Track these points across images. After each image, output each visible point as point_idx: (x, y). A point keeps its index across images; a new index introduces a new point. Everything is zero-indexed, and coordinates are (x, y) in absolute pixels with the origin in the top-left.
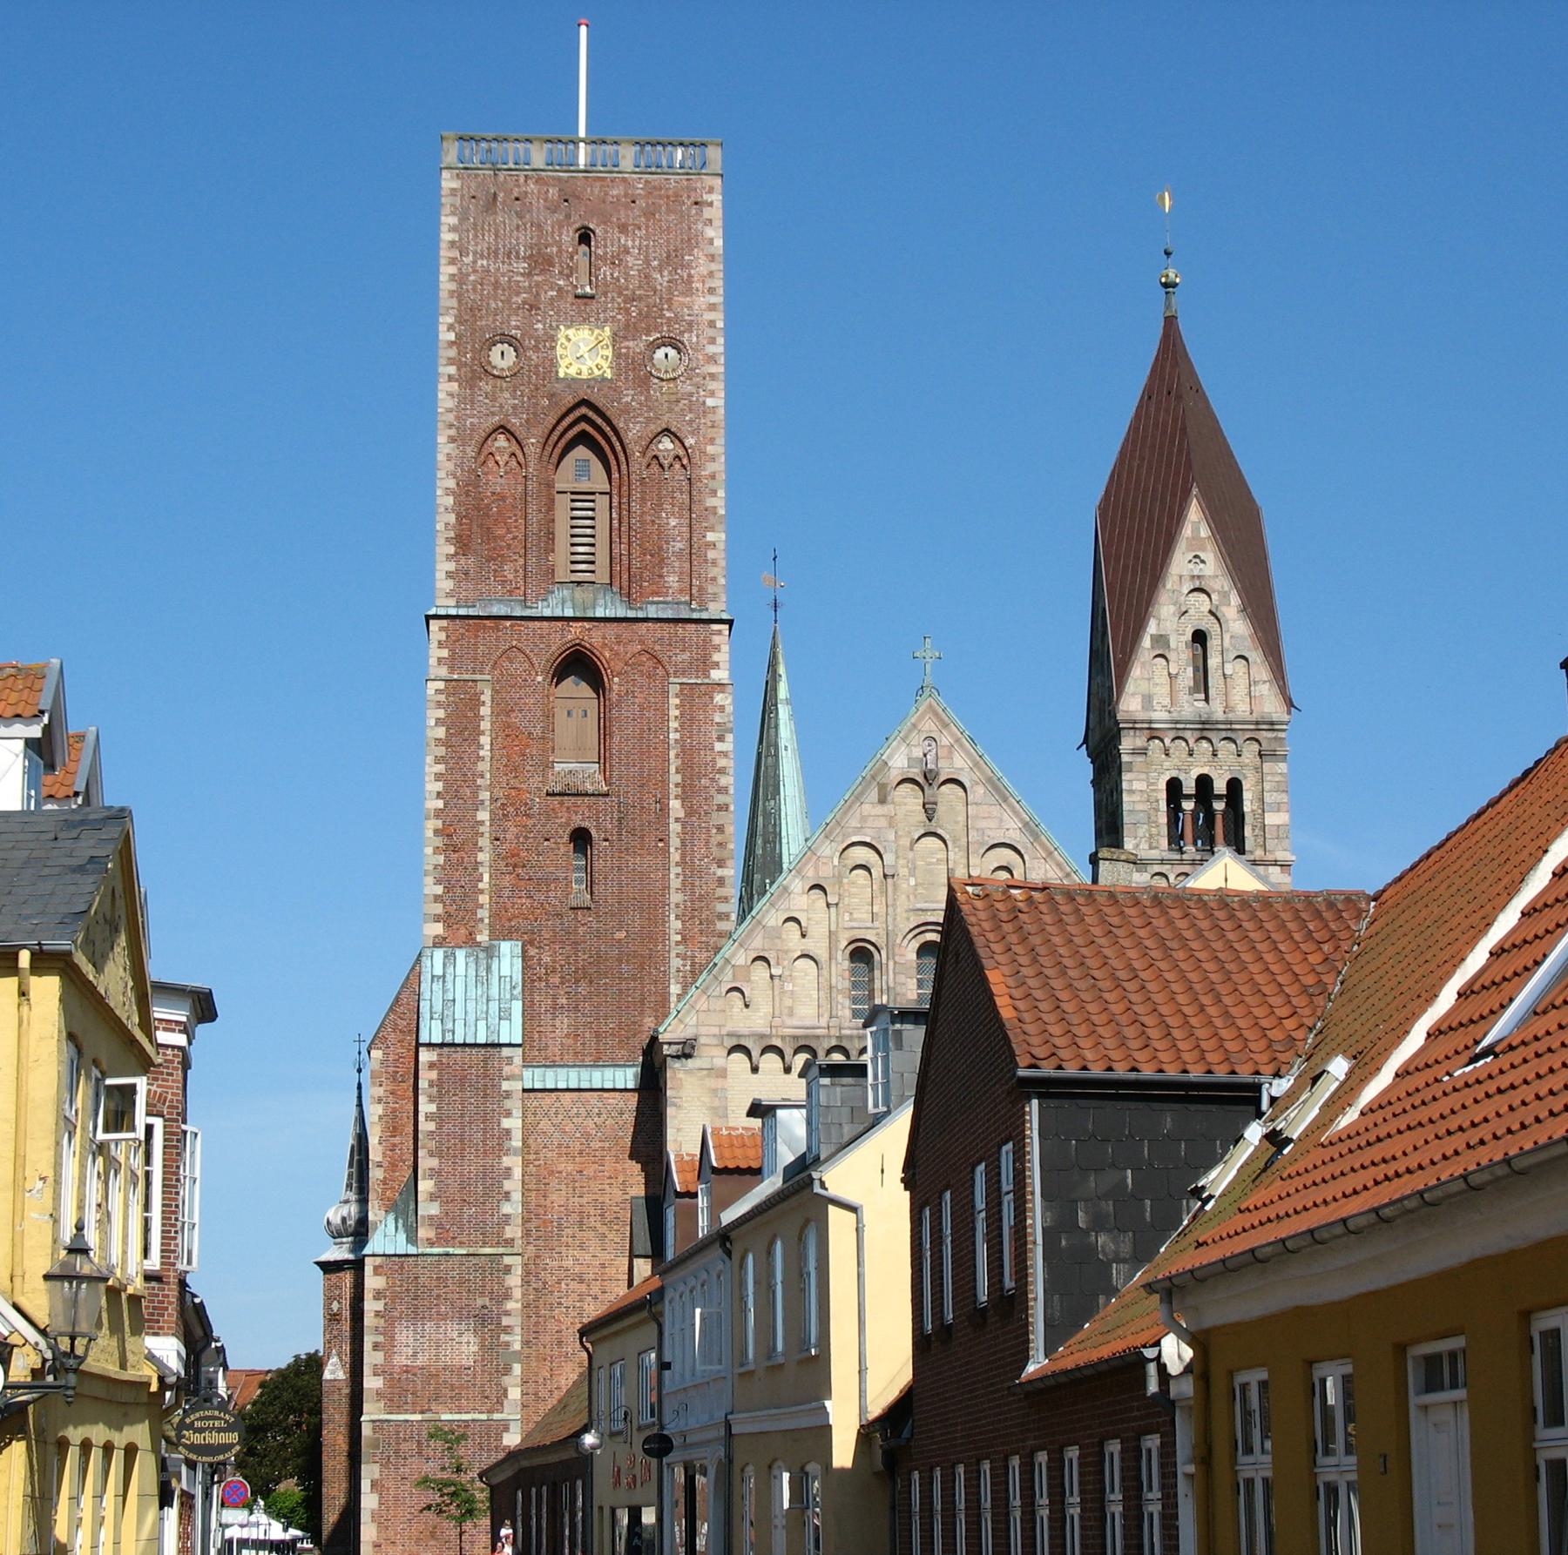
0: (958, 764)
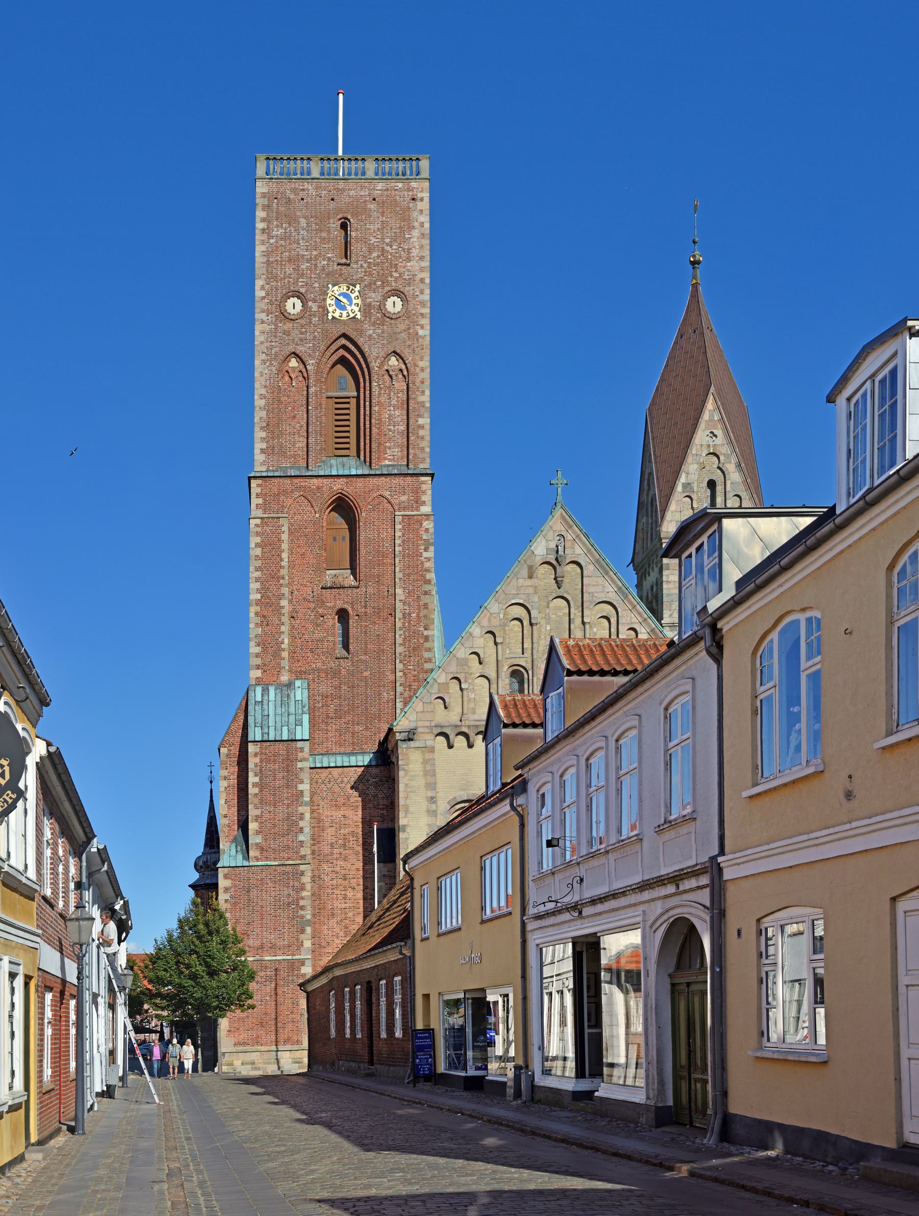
0: (577, 551)
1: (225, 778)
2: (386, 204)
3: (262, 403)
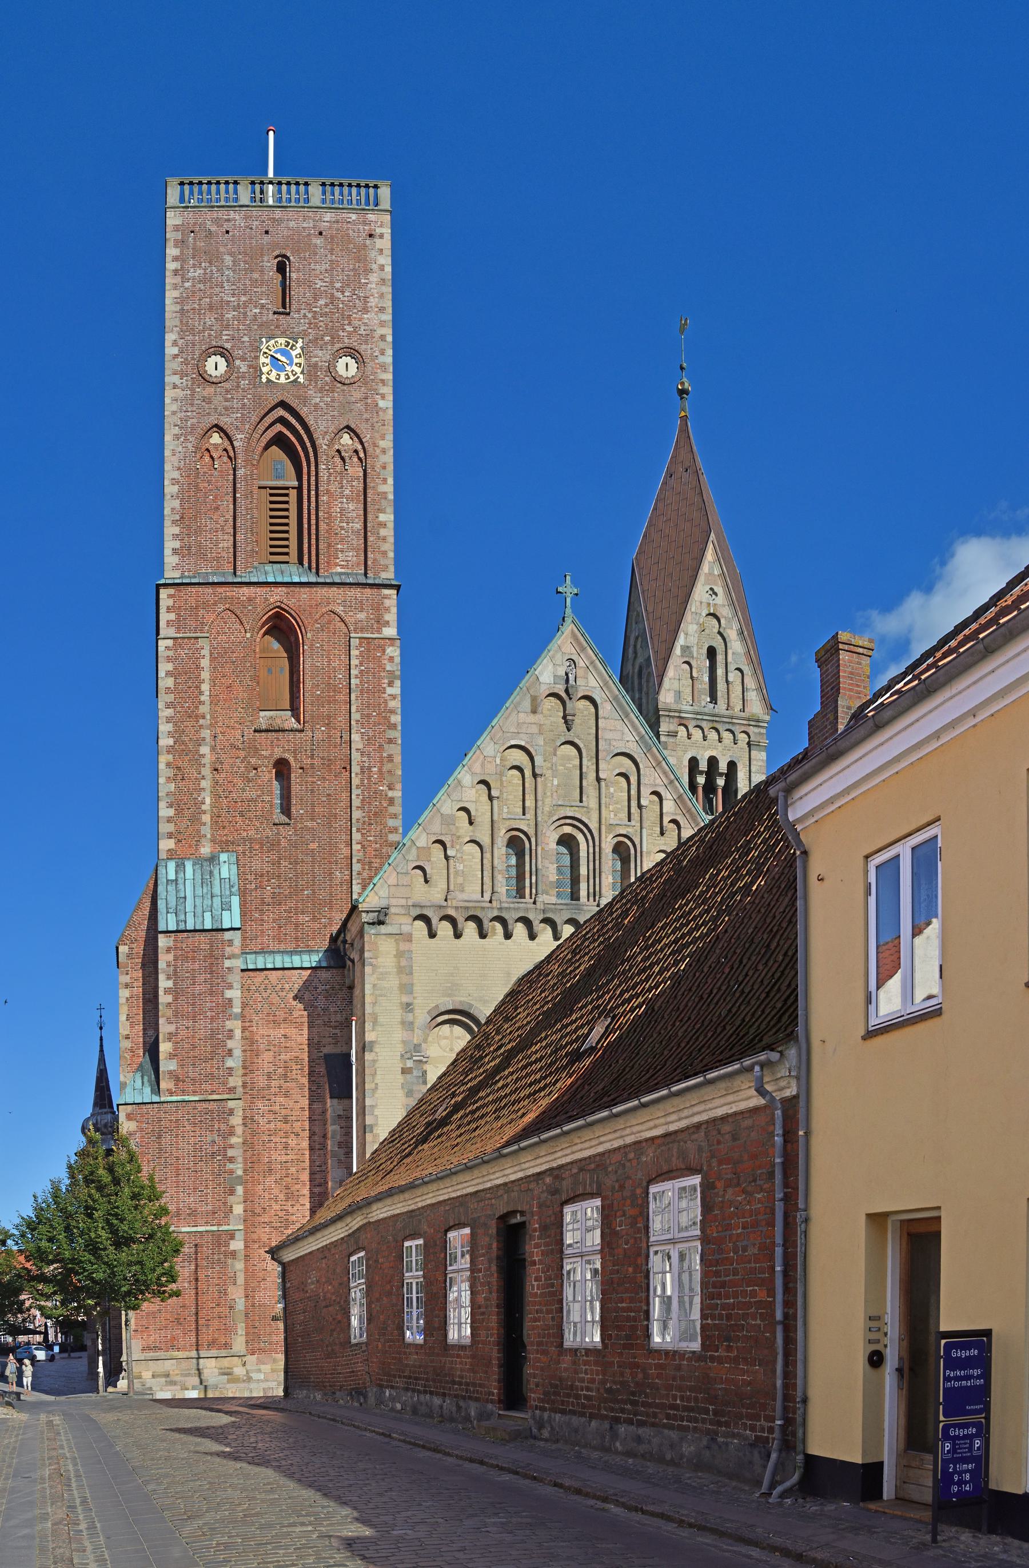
1: (127, 986)
2: (337, 240)
3: (175, 489)
